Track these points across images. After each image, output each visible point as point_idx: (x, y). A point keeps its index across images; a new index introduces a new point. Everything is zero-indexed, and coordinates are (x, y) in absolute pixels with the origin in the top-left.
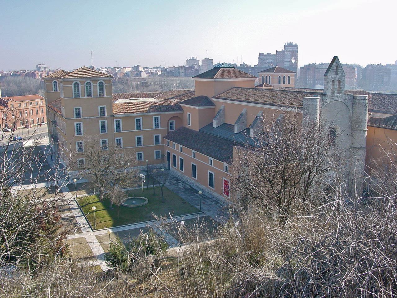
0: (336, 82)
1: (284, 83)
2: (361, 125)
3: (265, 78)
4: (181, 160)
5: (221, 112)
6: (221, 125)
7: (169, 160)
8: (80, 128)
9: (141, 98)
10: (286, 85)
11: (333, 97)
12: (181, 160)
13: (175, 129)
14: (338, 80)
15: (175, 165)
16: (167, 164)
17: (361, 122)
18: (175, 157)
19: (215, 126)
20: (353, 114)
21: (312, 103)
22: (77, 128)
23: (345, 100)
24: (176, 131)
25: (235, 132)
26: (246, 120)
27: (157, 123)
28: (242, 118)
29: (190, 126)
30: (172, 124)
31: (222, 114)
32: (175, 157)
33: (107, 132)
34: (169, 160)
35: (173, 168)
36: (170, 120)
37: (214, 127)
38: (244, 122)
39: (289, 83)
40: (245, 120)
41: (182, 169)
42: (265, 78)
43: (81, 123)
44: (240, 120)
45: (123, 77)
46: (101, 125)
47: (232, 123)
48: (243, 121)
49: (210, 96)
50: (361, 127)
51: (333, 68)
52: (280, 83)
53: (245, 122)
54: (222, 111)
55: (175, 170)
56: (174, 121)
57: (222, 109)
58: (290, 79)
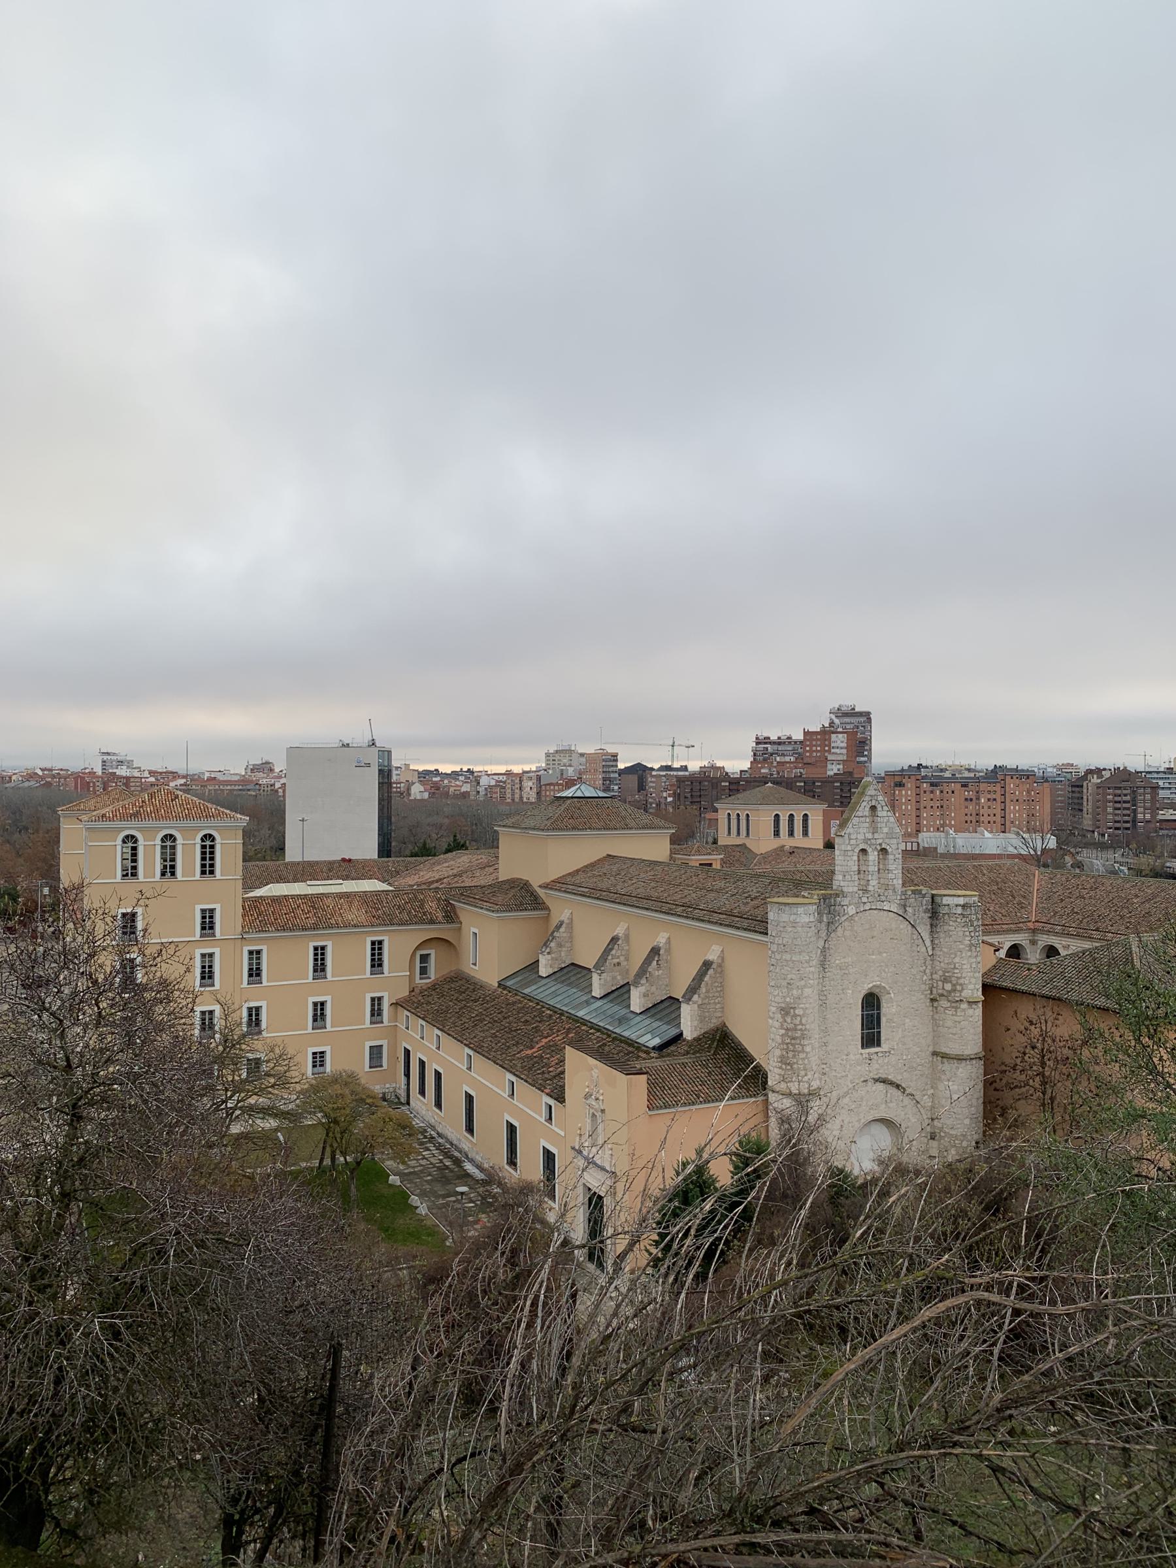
0: (873, 856)
1: (791, 833)
2: (961, 985)
3: (734, 817)
4: (438, 1075)
5: (562, 930)
6: (562, 969)
7: (407, 1075)
8: (258, 964)
9: (341, 881)
10: (799, 841)
11: (864, 899)
12: (438, 1075)
13: (433, 978)
14: (879, 848)
15: (422, 1092)
16: (403, 1087)
17: (959, 975)
18: (422, 1064)
19: (543, 971)
20: (933, 949)
21: (793, 917)
22: (250, 964)
23: (904, 906)
24: (434, 987)
25: (593, 994)
26: (627, 959)
27: (380, 959)
28: (613, 952)
29: (477, 968)
30: (424, 958)
31: (565, 935)
32: (422, 1064)
33: (217, 986)
34: (407, 1075)
35: (416, 1100)
36: (417, 948)
37: (540, 974)
38: (619, 964)
39: (805, 833)
40: (622, 958)
41: (438, 1104)
42: (734, 817)
43: (217, 951)
44: (610, 957)
45: (773, 1553)
46: (202, 962)
47: (590, 964)
48: (618, 960)
49: (535, 884)
50: (961, 991)
51: (859, 813)
52: (777, 833)
53: (624, 963)
54: (564, 925)
55: (422, 1108)
56: (432, 952)
57: (566, 921)
58: (810, 822)
